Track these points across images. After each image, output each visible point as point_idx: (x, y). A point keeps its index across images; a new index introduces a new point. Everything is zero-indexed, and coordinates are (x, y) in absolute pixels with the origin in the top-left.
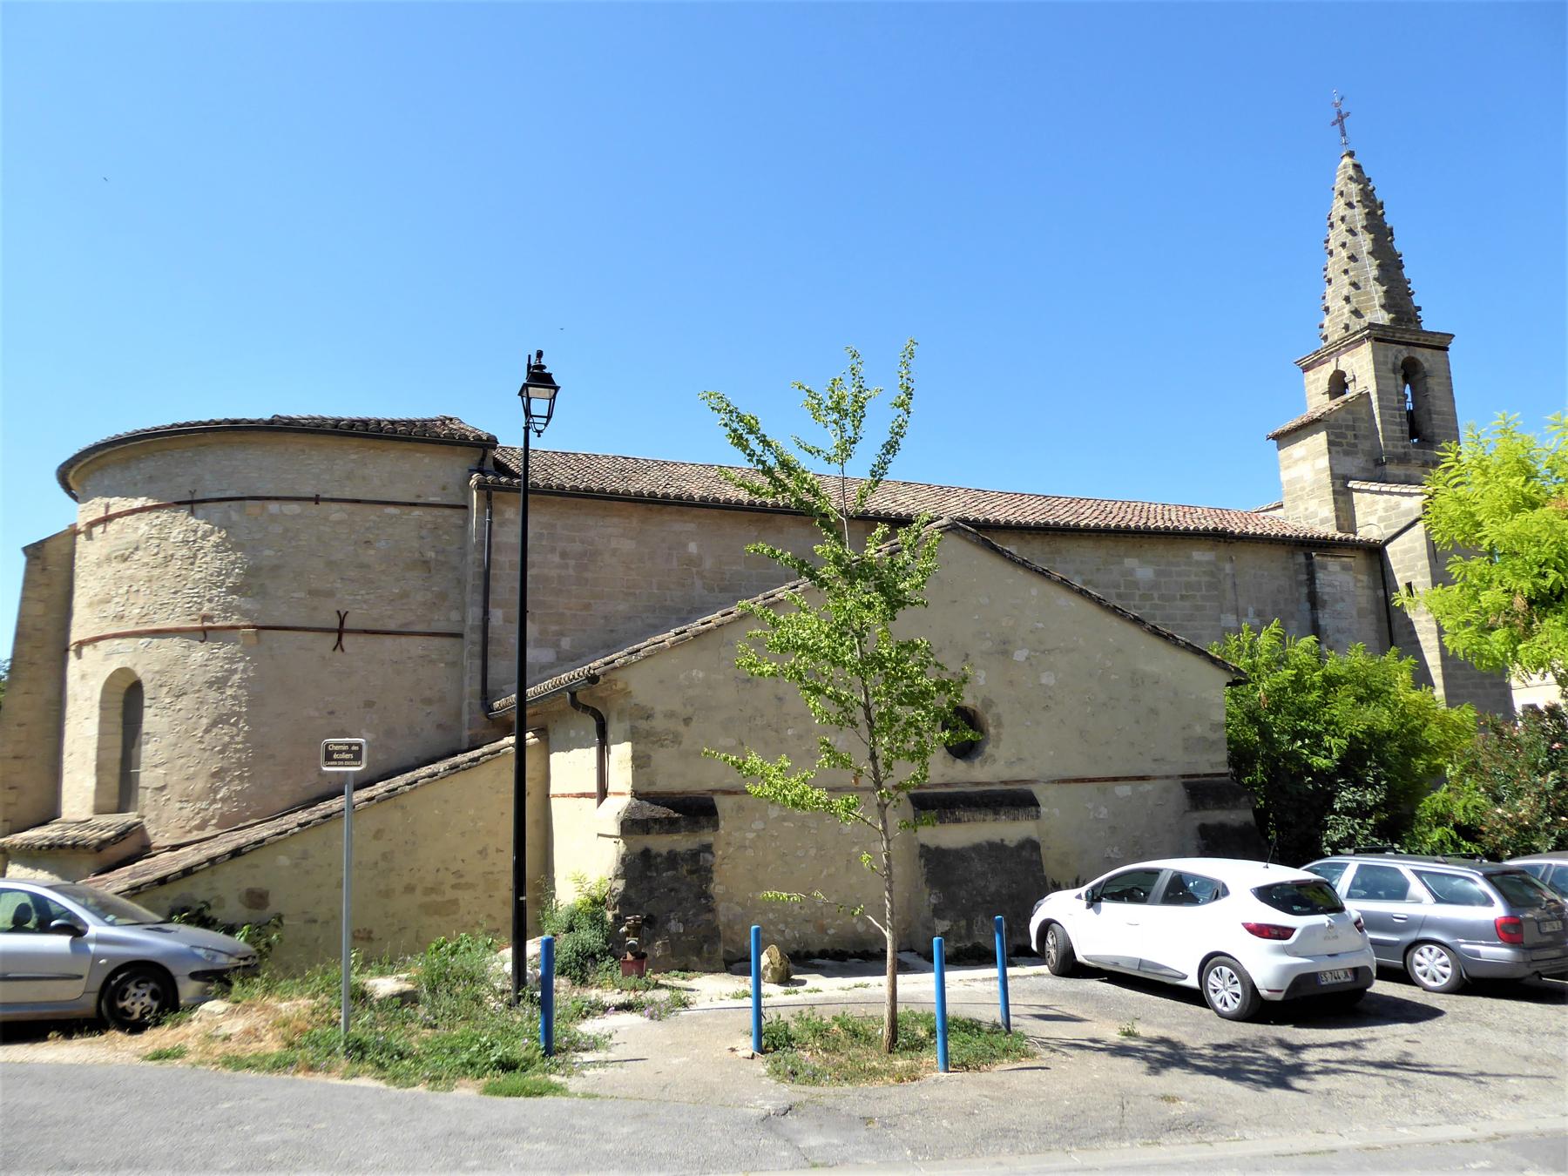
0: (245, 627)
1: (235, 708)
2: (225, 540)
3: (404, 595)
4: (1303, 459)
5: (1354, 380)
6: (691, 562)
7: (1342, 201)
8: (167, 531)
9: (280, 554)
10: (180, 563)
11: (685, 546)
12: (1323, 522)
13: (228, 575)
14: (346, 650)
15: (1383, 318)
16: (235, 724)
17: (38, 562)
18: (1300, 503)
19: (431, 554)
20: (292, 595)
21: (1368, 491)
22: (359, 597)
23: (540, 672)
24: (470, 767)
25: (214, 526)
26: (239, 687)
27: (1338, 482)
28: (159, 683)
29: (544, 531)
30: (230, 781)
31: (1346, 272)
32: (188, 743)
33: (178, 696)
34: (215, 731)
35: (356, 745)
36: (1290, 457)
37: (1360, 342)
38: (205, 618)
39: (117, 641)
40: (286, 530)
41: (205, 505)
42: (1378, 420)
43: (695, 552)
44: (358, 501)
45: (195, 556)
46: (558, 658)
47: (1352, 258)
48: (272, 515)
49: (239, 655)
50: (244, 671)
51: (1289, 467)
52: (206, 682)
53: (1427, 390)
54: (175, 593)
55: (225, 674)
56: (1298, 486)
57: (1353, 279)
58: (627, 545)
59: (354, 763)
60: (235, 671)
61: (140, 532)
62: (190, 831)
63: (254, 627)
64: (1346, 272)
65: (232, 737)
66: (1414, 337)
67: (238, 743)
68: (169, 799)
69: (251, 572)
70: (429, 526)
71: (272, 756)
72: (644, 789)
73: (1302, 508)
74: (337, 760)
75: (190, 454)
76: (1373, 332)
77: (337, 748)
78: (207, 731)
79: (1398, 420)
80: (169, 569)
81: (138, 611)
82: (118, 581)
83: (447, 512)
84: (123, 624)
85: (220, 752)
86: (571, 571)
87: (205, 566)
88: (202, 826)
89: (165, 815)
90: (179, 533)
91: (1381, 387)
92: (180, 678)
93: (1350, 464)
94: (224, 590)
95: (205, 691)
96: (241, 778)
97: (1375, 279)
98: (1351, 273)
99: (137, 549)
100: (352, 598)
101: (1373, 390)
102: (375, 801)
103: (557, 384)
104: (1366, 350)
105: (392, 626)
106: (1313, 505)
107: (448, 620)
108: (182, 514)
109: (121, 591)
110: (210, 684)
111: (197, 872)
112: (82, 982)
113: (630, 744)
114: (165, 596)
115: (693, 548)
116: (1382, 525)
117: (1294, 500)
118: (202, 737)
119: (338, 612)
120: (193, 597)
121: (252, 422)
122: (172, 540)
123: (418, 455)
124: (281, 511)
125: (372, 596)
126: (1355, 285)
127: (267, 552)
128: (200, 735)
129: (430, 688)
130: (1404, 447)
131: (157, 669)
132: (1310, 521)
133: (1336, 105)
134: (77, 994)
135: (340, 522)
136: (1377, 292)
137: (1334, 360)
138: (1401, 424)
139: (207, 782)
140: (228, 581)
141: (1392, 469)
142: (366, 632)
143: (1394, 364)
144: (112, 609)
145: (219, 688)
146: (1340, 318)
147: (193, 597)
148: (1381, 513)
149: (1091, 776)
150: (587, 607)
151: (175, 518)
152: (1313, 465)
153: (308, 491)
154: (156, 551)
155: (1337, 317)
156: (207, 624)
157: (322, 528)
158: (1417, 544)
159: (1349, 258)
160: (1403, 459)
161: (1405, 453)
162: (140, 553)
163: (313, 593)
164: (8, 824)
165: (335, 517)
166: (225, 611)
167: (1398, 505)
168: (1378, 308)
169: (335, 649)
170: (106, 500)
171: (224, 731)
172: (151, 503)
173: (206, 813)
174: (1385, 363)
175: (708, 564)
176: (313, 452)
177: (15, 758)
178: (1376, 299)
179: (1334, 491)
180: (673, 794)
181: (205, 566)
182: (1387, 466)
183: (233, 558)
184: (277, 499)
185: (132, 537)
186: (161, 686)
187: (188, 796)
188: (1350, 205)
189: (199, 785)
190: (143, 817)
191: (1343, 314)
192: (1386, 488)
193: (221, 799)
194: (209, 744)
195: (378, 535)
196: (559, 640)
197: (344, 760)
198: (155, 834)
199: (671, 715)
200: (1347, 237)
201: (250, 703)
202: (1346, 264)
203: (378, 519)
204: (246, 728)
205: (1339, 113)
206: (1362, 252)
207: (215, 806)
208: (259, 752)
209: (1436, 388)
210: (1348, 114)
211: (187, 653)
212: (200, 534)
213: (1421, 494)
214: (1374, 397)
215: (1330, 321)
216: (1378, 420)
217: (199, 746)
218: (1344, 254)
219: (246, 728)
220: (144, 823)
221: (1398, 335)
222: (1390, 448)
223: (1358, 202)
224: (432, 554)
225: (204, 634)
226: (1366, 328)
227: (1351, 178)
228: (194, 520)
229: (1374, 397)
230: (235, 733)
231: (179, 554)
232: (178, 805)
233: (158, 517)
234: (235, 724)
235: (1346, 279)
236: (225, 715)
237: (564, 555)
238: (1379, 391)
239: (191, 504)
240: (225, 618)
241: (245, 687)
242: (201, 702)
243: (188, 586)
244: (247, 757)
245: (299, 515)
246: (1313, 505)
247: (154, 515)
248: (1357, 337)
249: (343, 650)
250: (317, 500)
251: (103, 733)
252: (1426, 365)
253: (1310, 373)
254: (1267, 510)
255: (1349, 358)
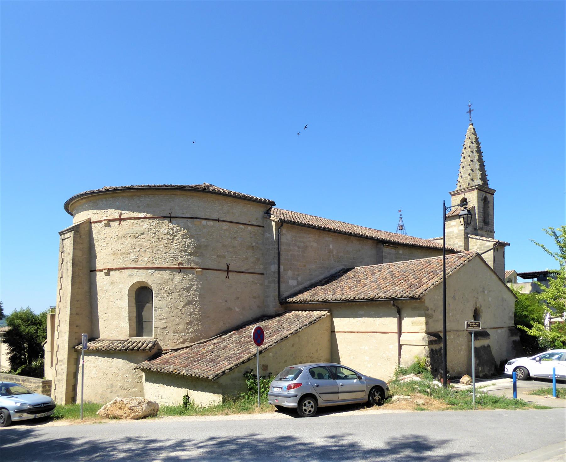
0: (197, 268)
1: (194, 299)
2: (186, 234)
3: (247, 258)
4: (455, 226)
5: (470, 202)
6: (330, 251)
7: (469, 141)
8: (158, 228)
9: (207, 241)
10: (166, 241)
11: (329, 246)
12: (459, 247)
13: (188, 248)
14: (230, 278)
15: (480, 182)
16: (195, 305)
17: (78, 233)
18: (452, 240)
19: (254, 244)
20: (212, 257)
21: (475, 238)
22: (233, 259)
23: (293, 289)
24: (315, 323)
25: (181, 228)
26: (195, 291)
27: (466, 235)
28: (160, 288)
29: (293, 238)
30: (194, 326)
31: (470, 165)
32: (176, 311)
33: (170, 294)
34: (187, 307)
35: (478, 322)
36: (450, 224)
37: (474, 189)
38: (180, 264)
39: (135, 270)
40: (209, 232)
41: (176, 219)
42: (477, 216)
43: (332, 248)
44: (232, 222)
45: (173, 239)
46: (298, 284)
47: (472, 161)
48: (204, 225)
49: (195, 279)
50: (197, 285)
51: (449, 228)
52: (182, 289)
53: (488, 207)
54: (165, 253)
55: (190, 286)
56: (452, 234)
57: (472, 168)
58: (315, 245)
59: (477, 327)
60: (194, 285)
61: (144, 227)
62: (178, 344)
63: (200, 268)
64: (470, 165)
65: (194, 310)
66: (487, 190)
67: (196, 312)
68: (168, 332)
69: (198, 247)
70: (253, 233)
71: (208, 317)
72: (428, 331)
73: (452, 241)
74: (471, 327)
75: (167, 197)
76: (479, 187)
77: (471, 323)
78: (183, 307)
79: (481, 216)
80: (161, 243)
81: (146, 259)
82: (133, 246)
83: (258, 228)
84: (139, 263)
85: (189, 315)
86: (301, 253)
87: (178, 243)
88: (183, 342)
89: (167, 338)
90: (165, 229)
91: (479, 205)
92: (169, 287)
93: (470, 229)
94: (187, 253)
95: (181, 292)
96: (198, 324)
97: (479, 169)
98: (471, 166)
99: (143, 234)
100: (231, 259)
101: (476, 206)
102: (293, 334)
103: (472, 214)
104: (476, 192)
105: (243, 270)
106: (457, 241)
107: (260, 268)
108: (166, 222)
109: (135, 250)
110: (184, 289)
111: (252, 359)
112: (365, 392)
113: (425, 318)
114: (160, 254)
115: (331, 247)
116: (478, 250)
117: (449, 239)
118: (182, 309)
119: (227, 264)
120: (174, 255)
121: (178, 187)
122: (162, 232)
123: (249, 206)
124: (207, 224)
125: (237, 258)
126: (472, 170)
127: (203, 240)
128: (181, 308)
129: (255, 293)
130: (482, 225)
131: (158, 282)
132: (455, 246)
133: (469, 106)
134: (363, 396)
135: (226, 230)
136: (478, 174)
137: (463, 194)
138: (482, 218)
139: (185, 326)
140: (188, 250)
141: (479, 232)
142: (236, 272)
143: (482, 198)
144: (131, 257)
145: (187, 291)
146: (466, 180)
147: (174, 255)
148: (478, 246)
149: (495, 327)
150: (305, 266)
151: (162, 223)
152: (458, 228)
153: (215, 217)
154: (154, 235)
155: (465, 180)
156: (181, 266)
157: (220, 232)
158: (490, 257)
159: (471, 160)
160: (482, 229)
161: (482, 227)
162: (144, 236)
163: (218, 256)
164: (77, 340)
165: (225, 227)
166: (188, 261)
167: (485, 244)
168: (478, 179)
169: (226, 278)
170: (120, 211)
171: (190, 308)
172: (149, 215)
173: (185, 337)
174: (480, 198)
175: (335, 253)
176: (216, 202)
177: (77, 314)
178: (478, 176)
179: (464, 237)
180: (432, 332)
181: (178, 243)
182: (478, 231)
183: (190, 241)
184: (205, 219)
185: (140, 229)
186: (161, 289)
187: (177, 331)
188: (472, 142)
189: (182, 327)
190: (157, 339)
191: (467, 179)
192: (481, 238)
193: (190, 332)
194: (185, 312)
195: (237, 235)
196: (298, 277)
197: (474, 327)
198: (163, 345)
199: (432, 309)
200: (470, 153)
201: (200, 297)
202: (470, 163)
203: (238, 230)
204: (199, 306)
205: (470, 109)
206: (475, 159)
207: (188, 335)
208: (204, 316)
209: (490, 207)
210: (473, 110)
211: (172, 277)
212: (175, 230)
213: (494, 241)
214: (476, 208)
215: (462, 181)
216: (477, 216)
217: (181, 312)
218: (469, 159)
219: (199, 306)
220: (158, 341)
221: (484, 189)
222: (479, 225)
223: (474, 142)
224: (254, 244)
225: (180, 270)
226: (477, 186)
227: (473, 133)
228: (171, 225)
229: (476, 208)
230: (194, 308)
231: (166, 238)
232: (172, 334)
233: (154, 222)
234: (195, 305)
235: (469, 168)
236: (190, 301)
237: (299, 247)
238: (478, 207)
239: (170, 218)
240: (189, 264)
241: (198, 291)
242: (180, 296)
243: (171, 251)
244: (200, 317)
245: (212, 226)
246: (457, 241)
247: (151, 221)
248: (473, 188)
249: (229, 278)
250: (218, 220)
251: (130, 306)
252: (489, 199)
253: (454, 197)
254: (433, 240)
255: (469, 194)
